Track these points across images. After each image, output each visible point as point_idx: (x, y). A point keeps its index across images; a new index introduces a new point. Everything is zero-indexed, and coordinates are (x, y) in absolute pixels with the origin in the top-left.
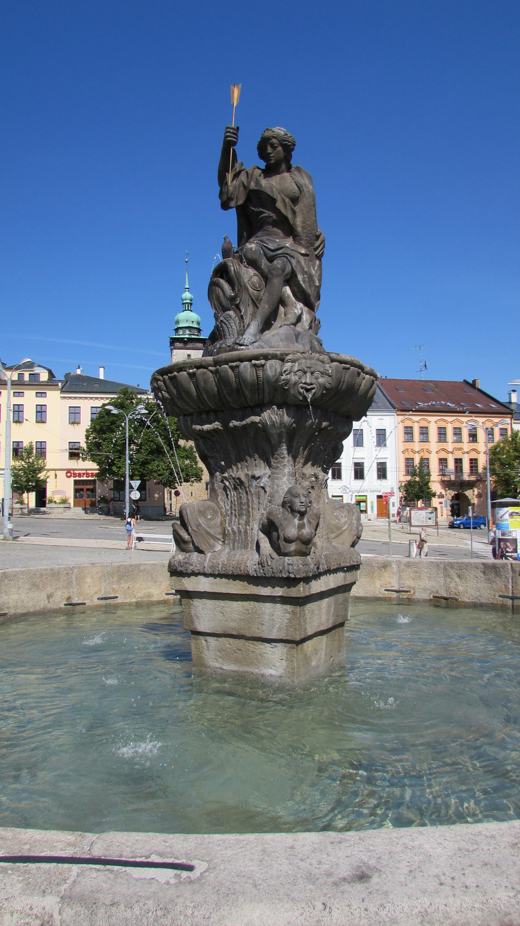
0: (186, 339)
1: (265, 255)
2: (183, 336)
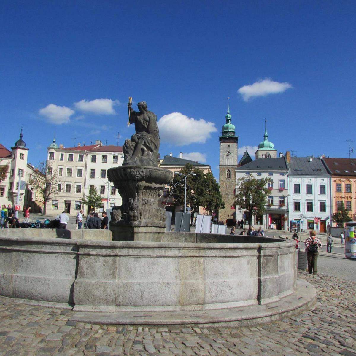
1: (137, 137)
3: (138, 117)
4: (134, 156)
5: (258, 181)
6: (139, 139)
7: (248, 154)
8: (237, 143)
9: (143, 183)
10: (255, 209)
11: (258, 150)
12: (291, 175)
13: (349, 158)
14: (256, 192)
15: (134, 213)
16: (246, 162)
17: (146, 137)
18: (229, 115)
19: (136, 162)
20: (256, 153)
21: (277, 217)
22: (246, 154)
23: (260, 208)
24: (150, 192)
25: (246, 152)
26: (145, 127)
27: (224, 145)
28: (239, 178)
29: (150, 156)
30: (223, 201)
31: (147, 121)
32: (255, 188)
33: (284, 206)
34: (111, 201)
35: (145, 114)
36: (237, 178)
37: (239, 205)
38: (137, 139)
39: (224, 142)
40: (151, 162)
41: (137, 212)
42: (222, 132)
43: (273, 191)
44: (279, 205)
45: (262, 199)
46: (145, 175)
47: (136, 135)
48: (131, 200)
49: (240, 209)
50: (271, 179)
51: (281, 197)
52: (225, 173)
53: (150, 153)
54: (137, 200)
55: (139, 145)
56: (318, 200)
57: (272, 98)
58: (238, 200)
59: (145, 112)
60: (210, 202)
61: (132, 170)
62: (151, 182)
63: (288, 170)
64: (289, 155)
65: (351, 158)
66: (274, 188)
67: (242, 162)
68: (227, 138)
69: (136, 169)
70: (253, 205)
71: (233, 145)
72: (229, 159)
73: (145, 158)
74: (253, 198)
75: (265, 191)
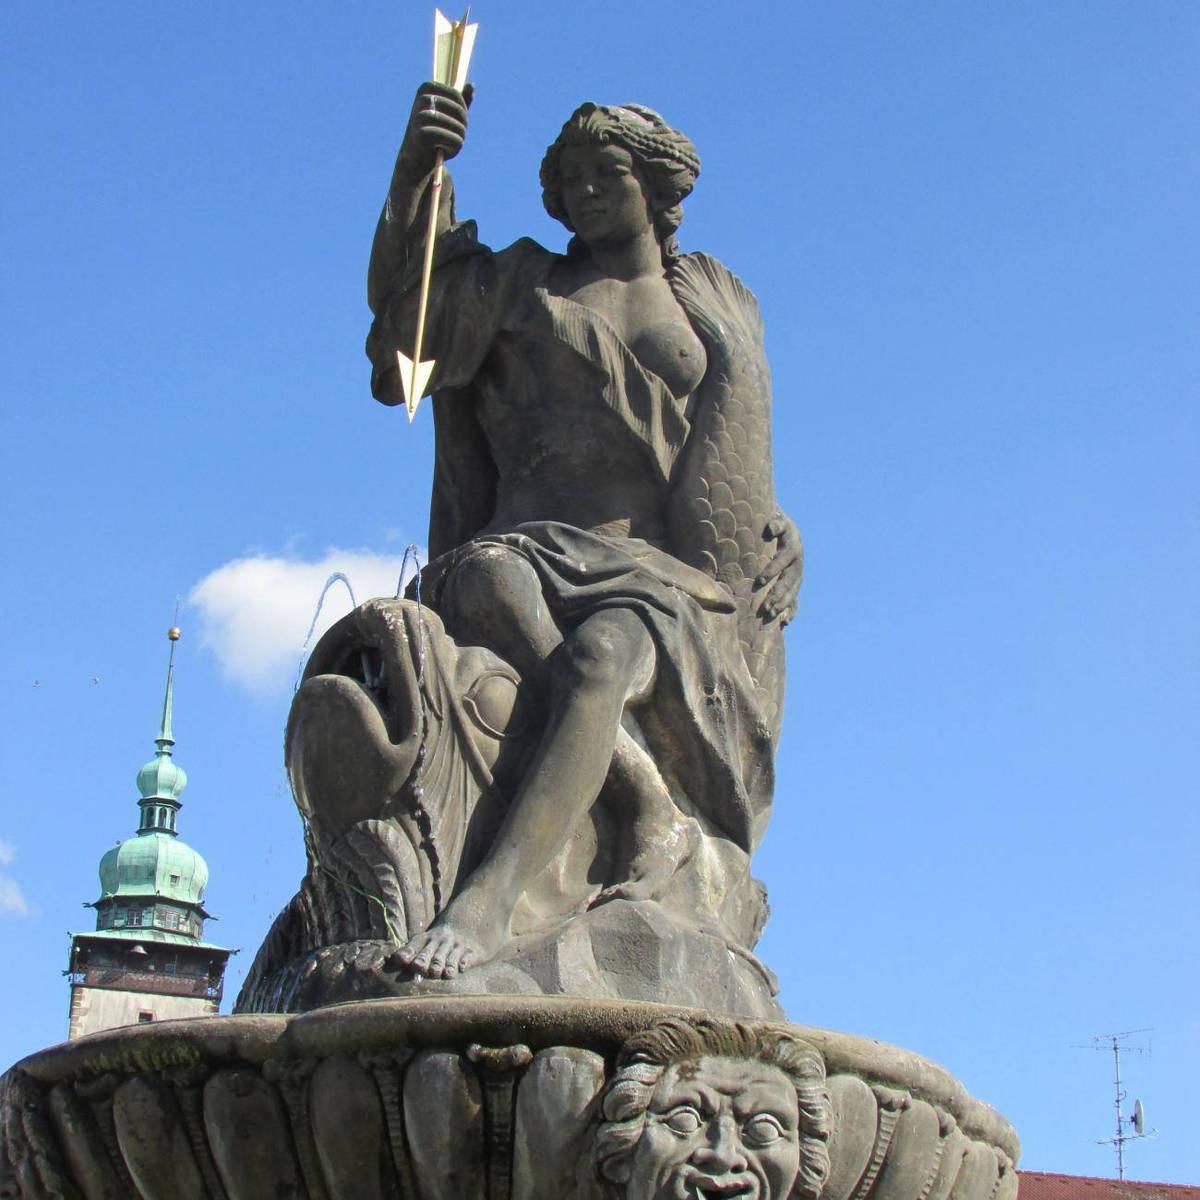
0: (141, 950)
1: (550, 592)
6: (570, 615)
13: (1113, 1175)
19: (541, 961)
26: (644, 454)
29: (707, 890)
35: (654, 278)
39: (105, 984)
42: (96, 899)
46: (816, 1184)
53: (709, 848)
61: (641, 1071)
65: (1126, 1177)
69: (707, 1061)
73: (648, 897)
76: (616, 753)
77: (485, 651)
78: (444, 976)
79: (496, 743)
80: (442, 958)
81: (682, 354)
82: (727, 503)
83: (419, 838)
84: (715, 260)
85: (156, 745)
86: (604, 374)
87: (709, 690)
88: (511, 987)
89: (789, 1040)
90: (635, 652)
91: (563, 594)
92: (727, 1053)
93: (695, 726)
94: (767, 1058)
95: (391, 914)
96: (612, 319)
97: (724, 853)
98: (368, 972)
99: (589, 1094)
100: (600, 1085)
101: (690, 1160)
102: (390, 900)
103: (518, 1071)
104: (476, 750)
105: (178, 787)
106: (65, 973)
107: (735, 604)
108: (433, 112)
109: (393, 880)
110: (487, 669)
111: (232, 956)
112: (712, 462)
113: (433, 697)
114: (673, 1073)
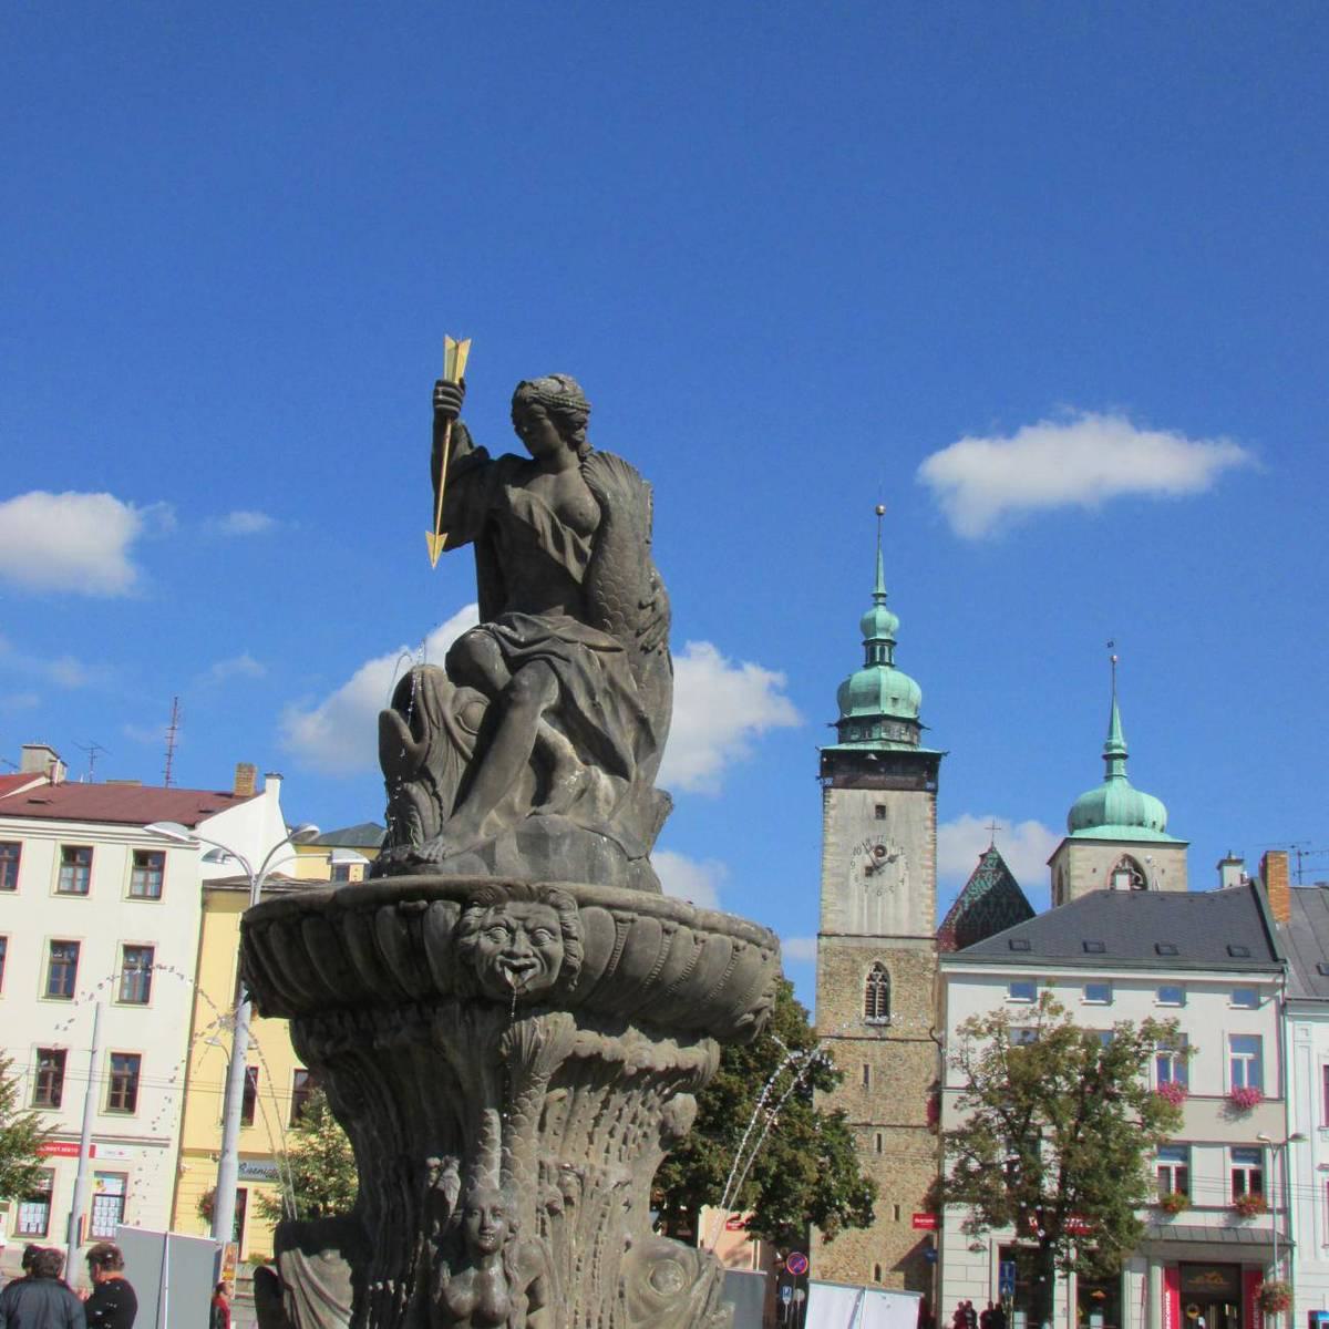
0: (873, 757)
1: (505, 654)
2: (861, 747)
3: (515, 494)
4: (473, 807)
5: (1091, 1040)
6: (515, 664)
7: (1000, 865)
8: (934, 791)
9: (558, 1032)
10: (1072, 1233)
11: (1067, 842)
12: (1301, 1003)
14: (1083, 1115)
15: (483, 1285)
16: (989, 918)
17: (578, 653)
18: (882, 615)
19: (487, 853)
20: (1051, 862)
21: (1214, 1282)
22: (994, 864)
23: (1113, 1223)
24: (605, 1104)
25: (992, 850)
27: (853, 802)
28: (970, 1021)
29: (601, 804)
30: (862, 1173)
31: (582, 531)
32: (1077, 1093)
33: (1266, 1210)
34: (106, 1157)
35: (572, 472)
36: (956, 1018)
37: (972, 1200)
38: (499, 670)
39: (847, 785)
40: (611, 858)
41: (508, 1278)
42: (836, 718)
43: (1188, 1109)
44: (1229, 1200)
45: (1121, 1167)
46: (576, 963)
47: (495, 635)
48: (441, 1170)
49: (974, 1232)
50: (1180, 1029)
51: (1240, 1151)
52: (856, 985)
53: (604, 781)
54: (492, 1175)
55: (516, 715)
56: (1317, 1165)
57: (1129, 519)
58: (961, 1167)
59: (571, 458)
60: (777, 1178)
61: (475, 911)
62: (613, 1027)
63: (1282, 972)
64: (1282, 872)
66: (1194, 1088)
67: (966, 914)
68: (870, 758)
69: (509, 905)
70: (1061, 1203)
71: (907, 804)
72: (879, 893)
73: (560, 817)
74: (1066, 1154)
75: (1144, 1110)
76: (539, 737)
77: (469, 688)
78: (435, 862)
79: (474, 738)
80: (434, 854)
81: (581, 514)
82: (613, 592)
83: (431, 790)
84: (611, 454)
85: (873, 598)
86: (536, 531)
87: (593, 698)
88: (472, 868)
89: (554, 891)
90: (544, 684)
91: (512, 655)
92: (521, 900)
93: (585, 719)
94: (543, 901)
95: (414, 831)
96: (545, 498)
97: (615, 783)
98: (399, 862)
99: (452, 923)
100: (458, 918)
101: (502, 953)
102: (415, 824)
103: (422, 913)
104: (460, 742)
105: (892, 629)
106: (818, 778)
107: (622, 647)
108: (441, 397)
109: (416, 813)
110: (469, 698)
111: (943, 758)
112: (602, 572)
113: (434, 717)
114: (491, 912)
